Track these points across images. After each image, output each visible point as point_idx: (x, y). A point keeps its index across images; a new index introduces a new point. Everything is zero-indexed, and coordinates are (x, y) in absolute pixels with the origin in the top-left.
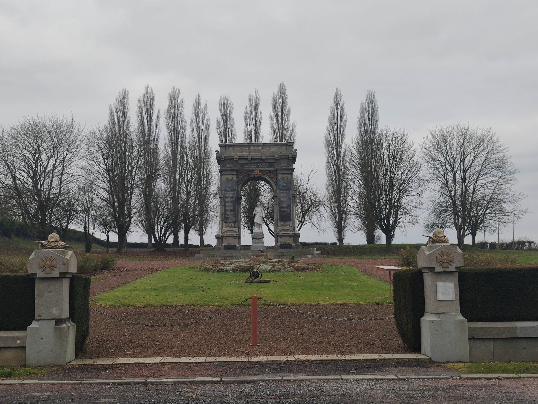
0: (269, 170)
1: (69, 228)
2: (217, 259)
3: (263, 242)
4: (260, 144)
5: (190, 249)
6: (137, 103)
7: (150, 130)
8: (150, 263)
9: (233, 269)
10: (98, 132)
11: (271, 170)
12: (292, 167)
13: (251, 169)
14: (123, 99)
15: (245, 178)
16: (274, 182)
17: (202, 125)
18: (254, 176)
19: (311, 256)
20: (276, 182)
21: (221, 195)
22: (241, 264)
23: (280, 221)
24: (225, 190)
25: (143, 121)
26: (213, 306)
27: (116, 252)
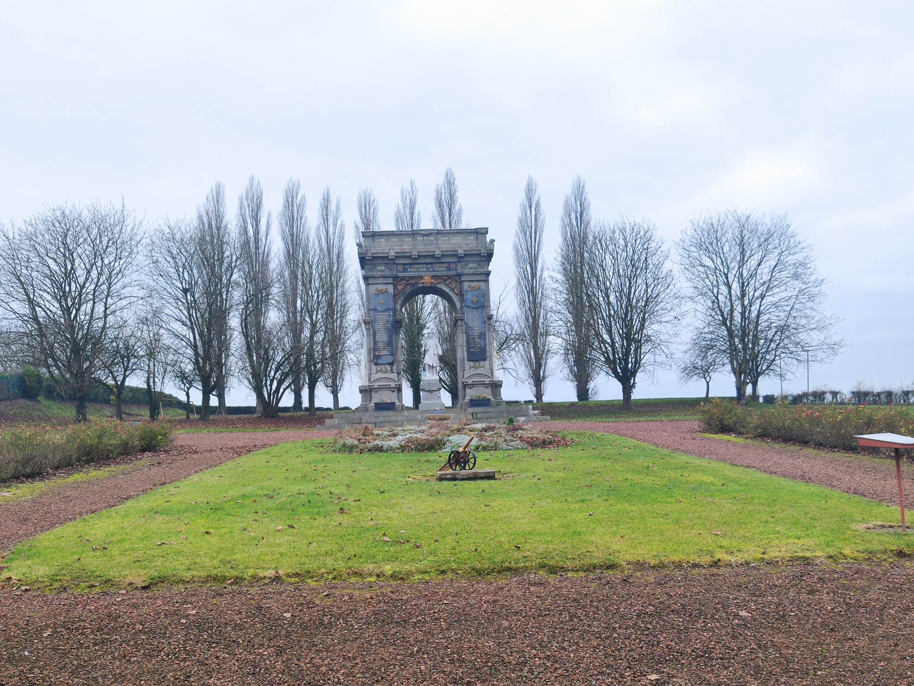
0: (449, 276)
1: (126, 384)
2: (366, 427)
3: (440, 397)
4: (432, 231)
5: (318, 412)
6: (237, 202)
7: (257, 240)
8: (260, 434)
9: (401, 446)
10: (167, 230)
11: (451, 275)
12: (486, 269)
13: (416, 274)
14: (217, 197)
15: (408, 290)
16: (457, 294)
17: (334, 233)
18: (421, 285)
19: (523, 418)
20: (461, 294)
21: (368, 319)
22: (415, 435)
23: (468, 360)
24: (375, 310)
25: (246, 228)
26: (378, 576)
27: (200, 419)
